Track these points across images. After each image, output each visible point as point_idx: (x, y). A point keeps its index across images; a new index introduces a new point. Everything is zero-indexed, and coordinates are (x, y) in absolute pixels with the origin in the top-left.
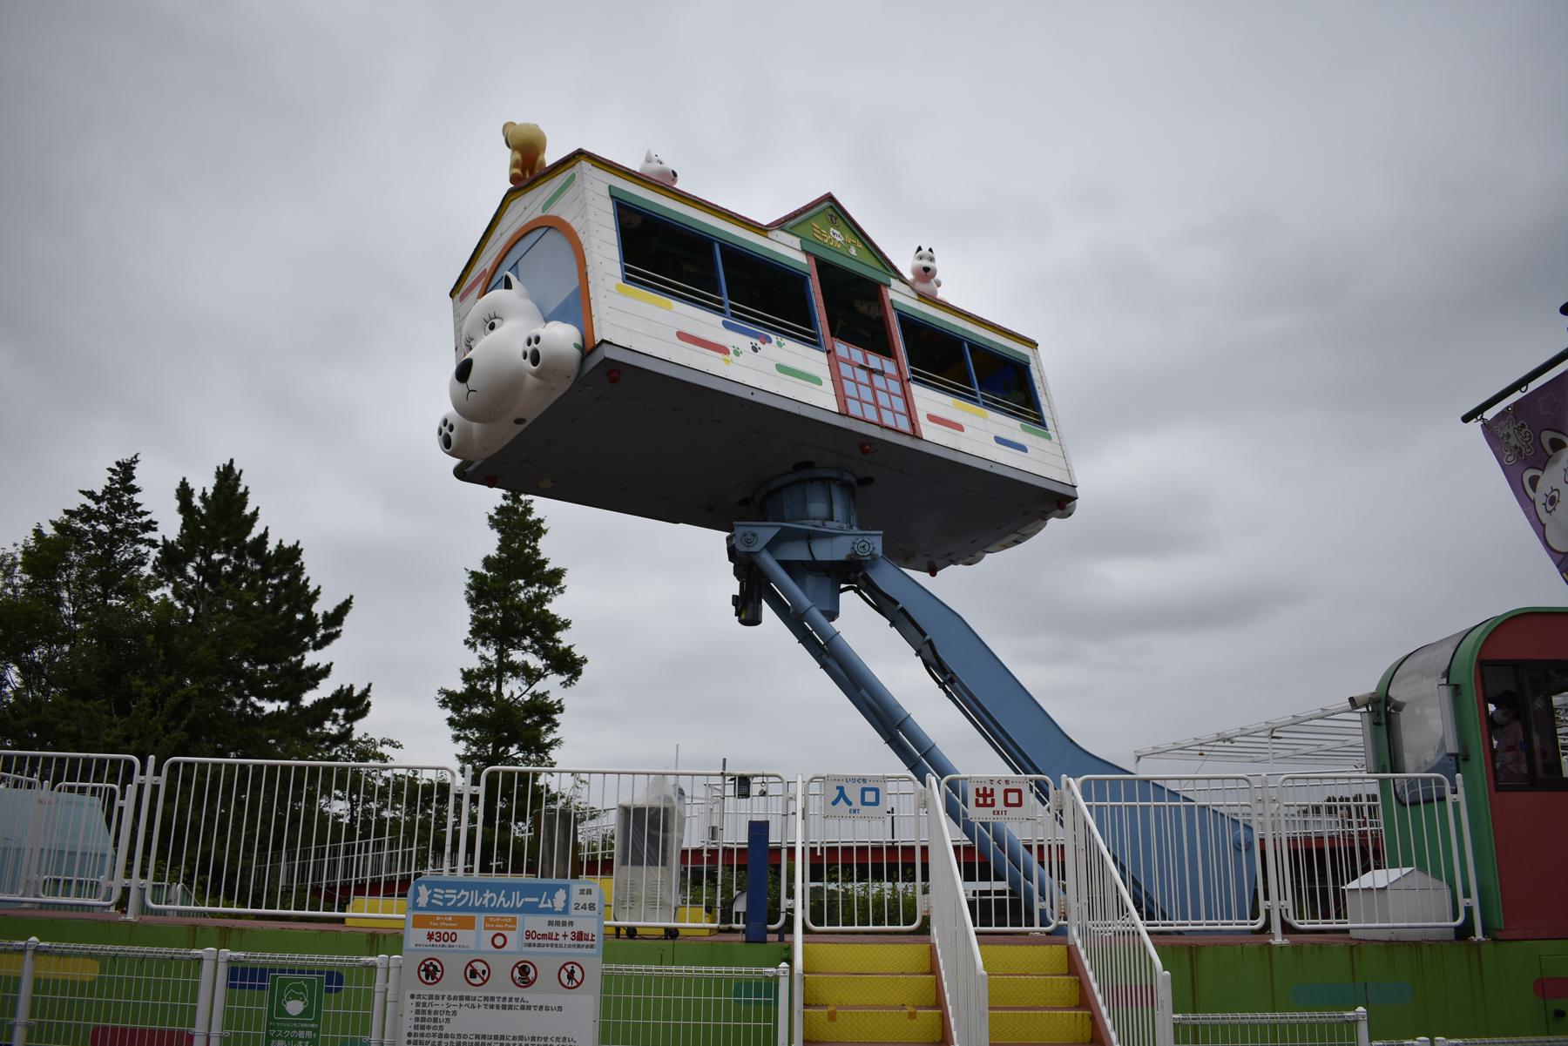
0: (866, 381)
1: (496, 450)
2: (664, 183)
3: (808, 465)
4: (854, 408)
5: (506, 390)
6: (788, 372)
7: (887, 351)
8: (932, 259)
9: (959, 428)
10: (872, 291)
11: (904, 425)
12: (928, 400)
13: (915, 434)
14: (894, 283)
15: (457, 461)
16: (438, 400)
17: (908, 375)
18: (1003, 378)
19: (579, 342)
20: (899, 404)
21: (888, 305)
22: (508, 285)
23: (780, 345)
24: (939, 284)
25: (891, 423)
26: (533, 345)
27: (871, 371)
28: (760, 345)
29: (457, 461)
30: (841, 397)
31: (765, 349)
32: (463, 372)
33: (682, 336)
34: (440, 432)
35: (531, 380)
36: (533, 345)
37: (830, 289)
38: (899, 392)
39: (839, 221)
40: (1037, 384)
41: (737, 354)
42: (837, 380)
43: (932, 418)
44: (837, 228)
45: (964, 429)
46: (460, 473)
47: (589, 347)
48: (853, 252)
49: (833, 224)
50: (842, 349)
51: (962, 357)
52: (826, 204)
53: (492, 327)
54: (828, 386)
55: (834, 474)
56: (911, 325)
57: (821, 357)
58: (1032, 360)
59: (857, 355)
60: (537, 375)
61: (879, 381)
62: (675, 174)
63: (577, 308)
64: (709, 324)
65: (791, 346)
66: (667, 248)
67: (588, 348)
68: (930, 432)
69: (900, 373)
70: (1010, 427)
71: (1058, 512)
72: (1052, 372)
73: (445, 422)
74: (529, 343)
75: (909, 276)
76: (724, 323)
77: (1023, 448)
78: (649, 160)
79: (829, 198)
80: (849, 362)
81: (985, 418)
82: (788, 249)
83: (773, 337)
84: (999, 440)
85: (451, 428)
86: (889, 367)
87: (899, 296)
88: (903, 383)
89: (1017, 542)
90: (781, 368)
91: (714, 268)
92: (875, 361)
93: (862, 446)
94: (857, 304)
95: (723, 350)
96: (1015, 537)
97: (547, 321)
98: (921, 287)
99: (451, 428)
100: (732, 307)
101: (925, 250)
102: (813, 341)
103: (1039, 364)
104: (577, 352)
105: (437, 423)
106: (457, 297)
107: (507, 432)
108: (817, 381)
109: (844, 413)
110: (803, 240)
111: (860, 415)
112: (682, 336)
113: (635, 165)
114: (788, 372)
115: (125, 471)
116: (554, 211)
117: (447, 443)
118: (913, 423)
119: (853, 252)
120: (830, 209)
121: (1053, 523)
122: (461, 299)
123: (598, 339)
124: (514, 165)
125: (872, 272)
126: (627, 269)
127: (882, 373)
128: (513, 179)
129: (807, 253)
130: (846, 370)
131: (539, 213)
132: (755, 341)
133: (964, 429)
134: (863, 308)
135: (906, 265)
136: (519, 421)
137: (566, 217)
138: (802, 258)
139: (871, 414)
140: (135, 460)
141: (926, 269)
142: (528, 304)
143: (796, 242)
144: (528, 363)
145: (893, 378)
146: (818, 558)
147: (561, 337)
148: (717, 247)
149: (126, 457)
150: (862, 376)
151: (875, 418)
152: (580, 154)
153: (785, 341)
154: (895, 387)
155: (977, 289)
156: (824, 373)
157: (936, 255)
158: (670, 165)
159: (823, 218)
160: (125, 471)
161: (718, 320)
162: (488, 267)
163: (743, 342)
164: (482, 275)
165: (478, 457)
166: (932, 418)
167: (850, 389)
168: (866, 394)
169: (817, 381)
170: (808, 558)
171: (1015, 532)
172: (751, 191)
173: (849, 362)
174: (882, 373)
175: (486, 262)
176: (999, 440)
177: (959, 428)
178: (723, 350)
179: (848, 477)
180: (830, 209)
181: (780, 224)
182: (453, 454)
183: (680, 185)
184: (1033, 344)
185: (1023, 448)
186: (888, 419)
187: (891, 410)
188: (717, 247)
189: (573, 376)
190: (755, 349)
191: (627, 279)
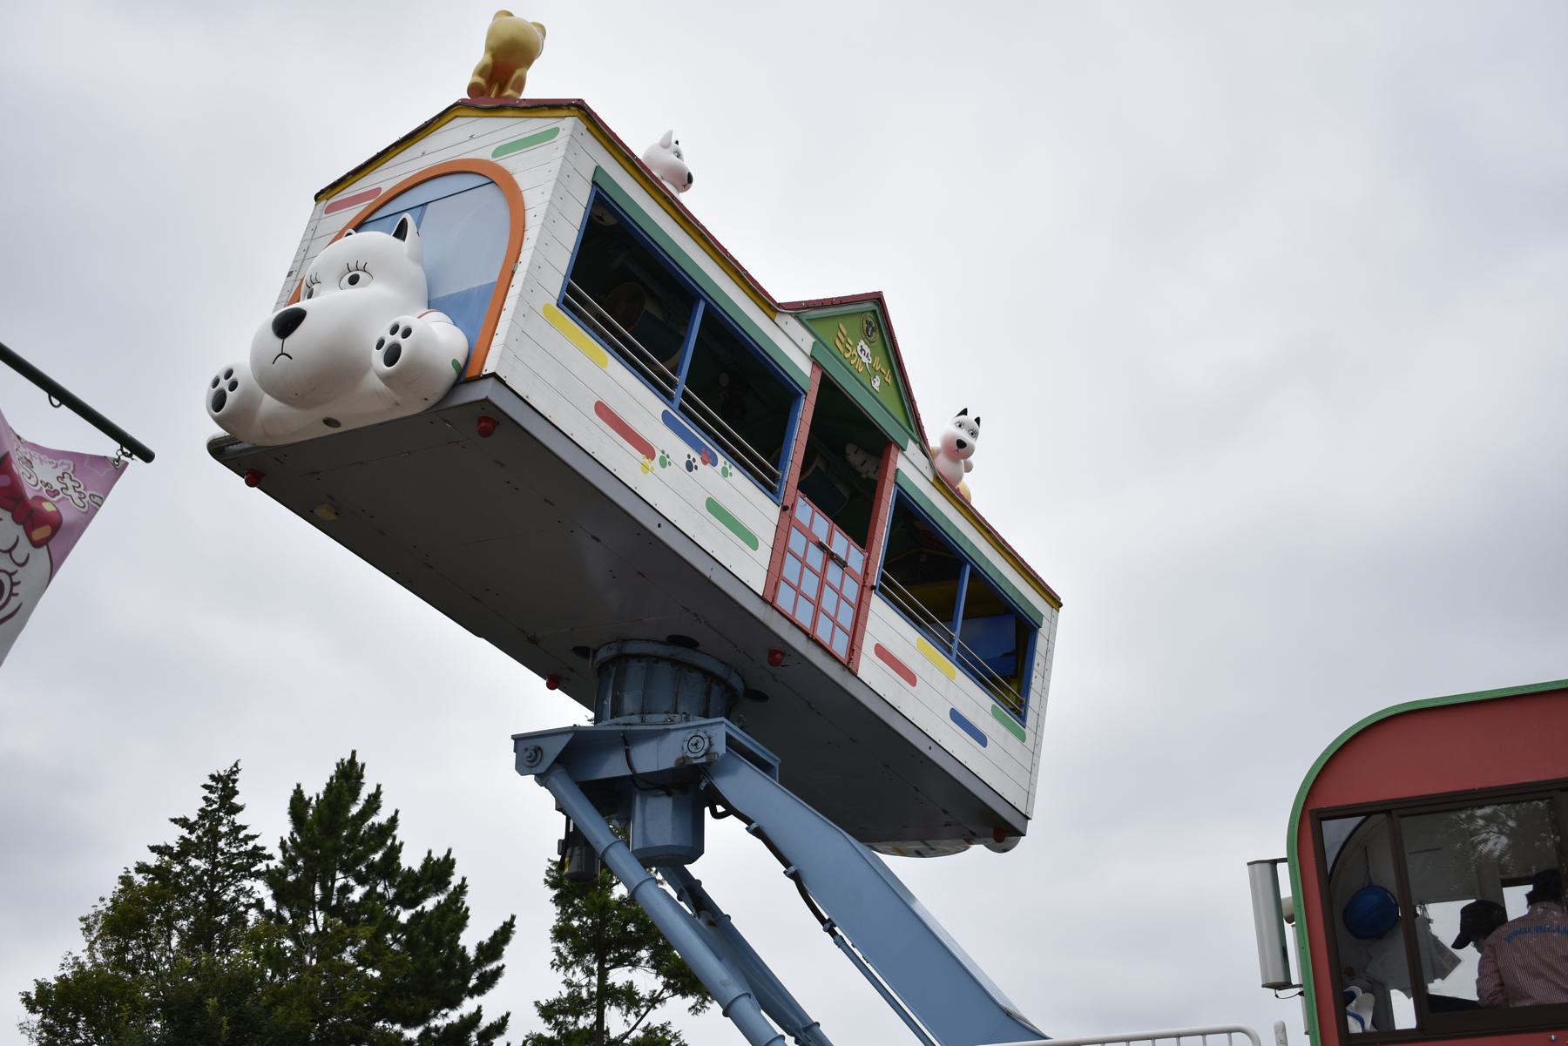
0: (818, 567)
1: (281, 443)
2: (664, 186)
3: (690, 644)
4: (785, 599)
5: (338, 372)
6: (719, 515)
7: (860, 535)
8: (974, 434)
9: (911, 678)
10: (880, 446)
11: (840, 647)
12: (887, 625)
13: (849, 667)
14: (912, 448)
15: (219, 432)
16: (238, 342)
17: (875, 580)
18: (999, 633)
19: (461, 361)
20: (846, 616)
21: (890, 475)
22: (401, 233)
23: (725, 473)
24: (969, 468)
25: (825, 639)
26: (398, 337)
27: (831, 556)
28: (699, 462)
29: (219, 432)
30: (775, 576)
31: (703, 469)
32: (287, 324)
33: (602, 410)
34: (216, 383)
35: (373, 382)
36: (398, 337)
37: (819, 420)
38: (853, 598)
39: (876, 336)
40: (1038, 659)
41: (663, 463)
42: (780, 550)
43: (881, 652)
44: (870, 343)
45: (915, 681)
46: (217, 449)
47: (472, 373)
48: (876, 384)
49: (867, 335)
50: (804, 510)
51: (957, 577)
52: (869, 306)
53: (354, 280)
54: (764, 554)
55: (719, 670)
56: (907, 510)
57: (773, 511)
58: (1045, 624)
59: (821, 526)
60: (386, 379)
61: (834, 573)
62: (690, 179)
63: (478, 311)
64: (643, 406)
65: (739, 478)
66: (635, 278)
67: (466, 374)
68: (871, 670)
69: (866, 573)
70: (977, 702)
71: (992, 841)
72: (1074, 665)
73: (229, 374)
74: (394, 330)
75: (934, 442)
76: (665, 415)
77: (981, 739)
78: (665, 145)
79: (878, 299)
80: (807, 532)
81: (950, 678)
82: (793, 349)
83: (721, 459)
84: (956, 716)
85: (233, 386)
86: (856, 559)
87: (909, 468)
88: (865, 588)
89: (919, 854)
90: (713, 507)
91: (687, 324)
92: (841, 544)
93: (772, 653)
94: (850, 449)
95: (647, 450)
96: (919, 846)
97: (432, 305)
98: (942, 463)
99: (233, 386)
100: (685, 396)
101: (971, 417)
102: (769, 484)
103: (1053, 633)
104: (452, 373)
105: (218, 370)
106: (323, 204)
107: (301, 424)
108: (752, 542)
109: (768, 601)
110: (819, 341)
111: (789, 610)
112: (602, 410)
113: (639, 148)
114: (719, 515)
115: (224, 788)
116: (509, 163)
117: (218, 402)
118: (853, 649)
119: (876, 384)
120: (871, 314)
121: (978, 851)
122: (329, 210)
123: (489, 368)
124: (481, 72)
125: (886, 418)
126: (569, 289)
127: (843, 564)
128: (473, 89)
129: (816, 363)
130: (797, 541)
131: (486, 154)
132: (694, 455)
133: (915, 681)
134: (855, 457)
135: (938, 427)
136: (329, 422)
137: (522, 180)
138: (805, 367)
139: (804, 616)
140: (235, 770)
141: (961, 444)
142: (416, 271)
143: (808, 341)
144: (378, 357)
145: (853, 576)
146: (639, 771)
147: (442, 339)
148: (702, 306)
149: (222, 768)
150: (816, 558)
151: (807, 624)
152: (579, 108)
153: (734, 470)
154: (851, 590)
155: (1019, 504)
156: (766, 536)
157: (982, 430)
158: (690, 164)
159: (857, 323)
160: (224, 788)
161: (658, 406)
162: (386, 187)
163: (679, 450)
164: (368, 197)
165: (253, 437)
166: (881, 652)
167: (791, 568)
168: (810, 584)
169: (752, 542)
170: (628, 772)
171: (923, 841)
172: (778, 243)
173: (807, 532)
174: (843, 564)
175: (386, 179)
176: (956, 716)
177: (911, 678)
178: (647, 450)
179: (735, 681)
180: (871, 314)
181: (799, 310)
182: (219, 421)
183: (686, 199)
184: (1056, 602)
185: (981, 739)
186: (823, 633)
187: (833, 620)
188: (702, 306)
189: (433, 400)
190: (690, 466)
191: (564, 304)
